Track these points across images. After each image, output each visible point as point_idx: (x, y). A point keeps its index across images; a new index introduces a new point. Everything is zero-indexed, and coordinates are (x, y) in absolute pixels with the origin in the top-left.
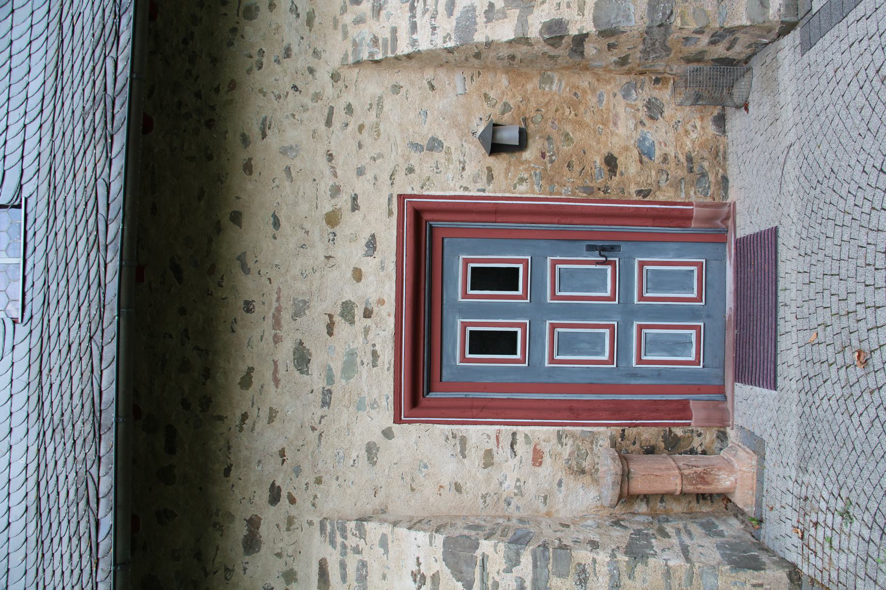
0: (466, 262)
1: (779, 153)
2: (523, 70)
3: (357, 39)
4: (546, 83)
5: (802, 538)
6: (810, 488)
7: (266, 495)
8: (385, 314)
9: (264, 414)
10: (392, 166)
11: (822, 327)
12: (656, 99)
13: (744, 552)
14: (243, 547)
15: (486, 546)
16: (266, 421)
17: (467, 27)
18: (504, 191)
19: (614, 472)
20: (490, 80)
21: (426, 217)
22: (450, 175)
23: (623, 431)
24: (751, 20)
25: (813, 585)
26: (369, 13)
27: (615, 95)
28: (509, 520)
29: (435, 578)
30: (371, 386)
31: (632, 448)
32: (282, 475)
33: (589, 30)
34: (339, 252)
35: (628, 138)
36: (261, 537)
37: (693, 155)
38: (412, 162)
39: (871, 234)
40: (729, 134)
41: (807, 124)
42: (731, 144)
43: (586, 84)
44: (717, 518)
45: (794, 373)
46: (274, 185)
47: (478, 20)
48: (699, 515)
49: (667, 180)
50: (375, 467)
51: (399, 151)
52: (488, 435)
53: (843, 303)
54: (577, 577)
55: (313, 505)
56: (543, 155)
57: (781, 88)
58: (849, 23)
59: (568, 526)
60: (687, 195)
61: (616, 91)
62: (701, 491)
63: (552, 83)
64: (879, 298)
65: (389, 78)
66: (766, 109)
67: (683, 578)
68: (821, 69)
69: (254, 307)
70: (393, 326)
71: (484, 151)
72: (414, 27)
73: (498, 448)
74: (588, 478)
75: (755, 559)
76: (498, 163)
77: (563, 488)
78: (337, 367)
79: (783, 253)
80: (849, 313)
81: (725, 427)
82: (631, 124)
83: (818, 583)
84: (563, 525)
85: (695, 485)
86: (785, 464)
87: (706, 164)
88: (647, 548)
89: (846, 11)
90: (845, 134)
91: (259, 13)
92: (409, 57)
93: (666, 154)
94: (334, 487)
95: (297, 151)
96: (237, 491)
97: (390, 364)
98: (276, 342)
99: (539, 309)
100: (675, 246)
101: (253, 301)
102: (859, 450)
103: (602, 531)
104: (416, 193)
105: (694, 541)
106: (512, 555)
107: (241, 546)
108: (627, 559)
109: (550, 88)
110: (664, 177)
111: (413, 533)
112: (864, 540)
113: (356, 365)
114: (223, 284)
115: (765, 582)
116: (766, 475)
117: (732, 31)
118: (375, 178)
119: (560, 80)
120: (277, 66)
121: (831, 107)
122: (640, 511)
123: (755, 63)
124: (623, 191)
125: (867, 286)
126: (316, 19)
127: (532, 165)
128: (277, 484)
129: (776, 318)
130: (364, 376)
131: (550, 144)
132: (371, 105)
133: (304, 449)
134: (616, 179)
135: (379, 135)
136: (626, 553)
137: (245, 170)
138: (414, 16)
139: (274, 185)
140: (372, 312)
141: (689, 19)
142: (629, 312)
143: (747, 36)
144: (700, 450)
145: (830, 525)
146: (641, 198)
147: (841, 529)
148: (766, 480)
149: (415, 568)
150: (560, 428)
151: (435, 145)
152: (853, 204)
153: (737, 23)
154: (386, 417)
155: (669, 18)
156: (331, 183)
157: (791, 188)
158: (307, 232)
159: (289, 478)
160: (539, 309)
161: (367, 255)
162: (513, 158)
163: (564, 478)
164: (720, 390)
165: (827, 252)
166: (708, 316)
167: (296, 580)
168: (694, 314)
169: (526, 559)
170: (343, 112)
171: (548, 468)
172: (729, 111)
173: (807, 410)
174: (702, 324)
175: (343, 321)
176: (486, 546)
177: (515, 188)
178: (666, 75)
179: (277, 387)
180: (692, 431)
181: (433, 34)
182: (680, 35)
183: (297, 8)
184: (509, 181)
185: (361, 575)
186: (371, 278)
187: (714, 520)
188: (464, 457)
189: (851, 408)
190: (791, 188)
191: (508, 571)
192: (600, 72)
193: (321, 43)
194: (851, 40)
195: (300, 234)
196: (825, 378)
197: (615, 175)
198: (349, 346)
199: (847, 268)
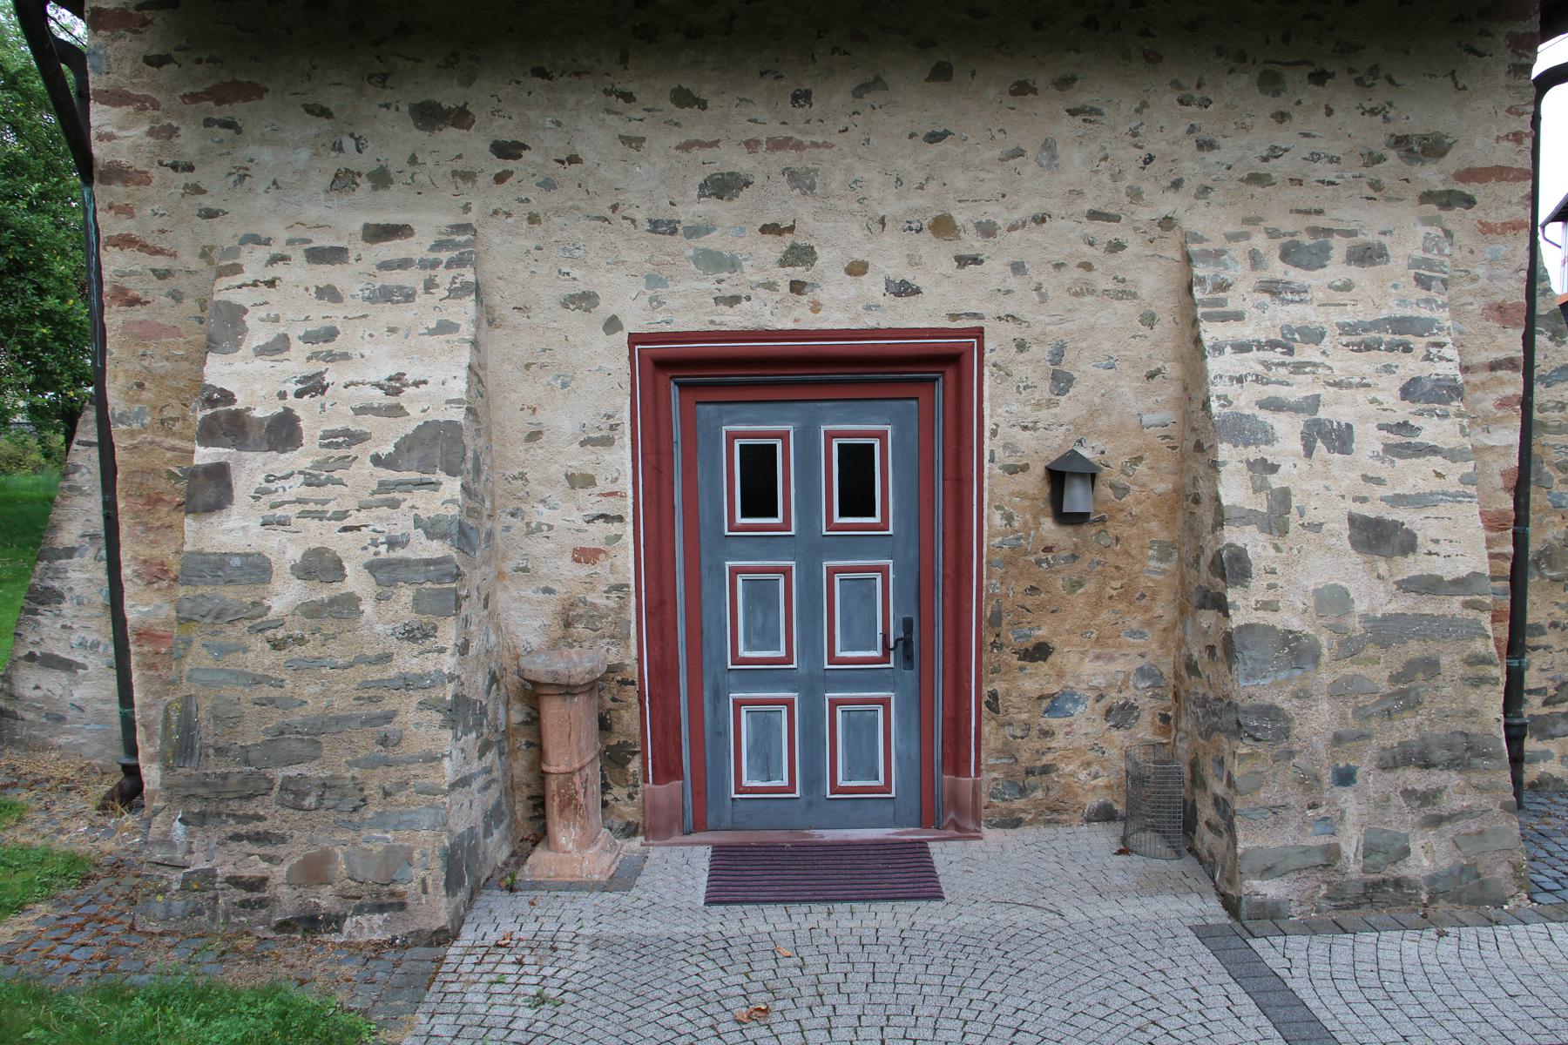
0: (882, 436)
1: (1051, 900)
2: (1179, 515)
3: (1225, 257)
4: (1160, 550)
5: (498, 946)
6: (570, 953)
7: (507, 136)
8: (796, 314)
9: (634, 129)
10: (1028, 317)
11: (800, 963)
12: (1137, 718)
13: (467, 867)
14: (422, 103)
15: (452, 487)
16: (623, 132)
17: (1241, 432)
18: (991, 492)
19: (573, 673)
20: (1163, 464)
21: (950, 372)
22: (1015, 407)
23: (633, 683)
24: (1244, 855)
25: (433, 961)
26: (1266, 275)
27: (1142, 656)
28: (490, 516)
29: (397, 411)
30: (686, 296)
31: (607, 697)
32: (539, 160)
33: (1234, 618)
35: (1078, 678)
36: (440, 130)
37: (1053, 775)
38: (1034, 348)
39: (930, 1021)
40: (1085, 828)
41: (1091, 936)
42: (1070, 830)
43: (1160, 612)
44: (509, 827)
45: (733, 928)
46: (995, 131)
47: (1253, 448)
48: (511, 800)
49: (1015, 737)
50: (559, 306)
51: (1051, 328)
52: (617, 479)
53: (834, 988)
54: (415, 626)
55: (495, 212)
56: (1048, 549)
57: (1146, 900)
58: (1226, 986)
59: (486, 607)
60: (992, 768)
61: (1149, 657)
62: (549, 801)
63: (1160, 560)
64: (843, 1033)
65: (1166, 309)
66: (1117, 880)
67: (426, 781)
68: (1168, 952)
69: (802, 106)
70: (779, 327)
71: (1053, 459)
72: (1242, 348)
73: (599, 495)
74: (558, 632)
75: (460, 883)
76: (1034, 482)
77: (541, 595)
78: (713, 242)
79: (905, 909)
80: (821, 996)
81: (644, 833)
82: (1099, 681)
83: (438, 968)
84: (486, 600)
85: (559, 793)
86: (599, 919)
87: (1039, 794)
88: (465, 726)
89: (1244, 982)
90: (1072, 985)
91: (1269, 97)
92: (1197, 341)
93: (1053, 734)
94: (525, 243)
95: (1049, 167)
96: (510, 89)
97: (721, 324)
98: (747, 143)
99: (812, 549)
100: (915, 751)
101: (811, 105)
102: (631, 1014)
103: (482, 658)
104: (987, 355)
105: (477, 795)
106: (443, 527)
107: (424, 99)
108: (449, 698)
109: (1152, 558)
110: (1019, 733)
111: (463, 373)
112: (510, 1022)
113: (717, 271)
114: (837, 55)
115: (431, 897)
116: (580, 894)
117: (1231, 828)
118: (1008, 292)
119: (1164, 572)
120: (1184, 128)
121: (1111, 967)
122: (512, 712)
123: (1189, 863)
124: (995, 671)
125: (859, 1017)
126: (1260, 189)
127: (1032, 533)
128: (525, 153)
129: (810, 901)
130: (701, 285)
131: (1065, 560)
132: (1123, 281)
133: (583, 195)
134: (1014, 661)
135: (1076, 294)
136: (456, 696)
137: (1018, 83)
138: (1260, 347)
139: (995, 131)
140: (800, 293)
141: (1249, 765)
142: (812, 685)
143: (1224, 850)
144: (608, 797)
145: (522, 981)
146: (986, 698)
147: (518, 995)
148: (573, 894)
149: (409, 378)
150: (633, 588)
152: (974, 997)
153: (1240, 835)
154: (638, 320)
155: (1250, 736)
156: (999, 222)
157: (998, 917)
158: (921, 187)
159: (535, 171)
160: (812, 549)
161: (888, 282)
162: (1043, 504)
163: (557, 595)
164: (700, 825)
165: (906, 967)
166: (810, 804)
167: (375, 188)
168: (812, 781)
169: (437, 549)
171: (569, 572)
172: (1119, 827)
173: (681, 946)
174: (797, 794)
175: (784, 249)
176: (452, 487)
177: (997, 508)
178: (1174, 732)
179: (678, 148)
180: (636, 786)
181: (1231, 379)
182: (1227, 752)
183: (1277, 157)
184: (1007, 498)
185: (392, 293)
186: (853, 291)
187: (506, 822)
188: (583, 444)
189: (689, 1003)
190: (998, 917)
191: (418, 522)
192: (1178, 633)
193: (1221, 199)
194: (1202, 990)
195: (919, 177)
196: (728, 969)
197: (1019, 659)
198: (745, 260)
199: (883, 992)
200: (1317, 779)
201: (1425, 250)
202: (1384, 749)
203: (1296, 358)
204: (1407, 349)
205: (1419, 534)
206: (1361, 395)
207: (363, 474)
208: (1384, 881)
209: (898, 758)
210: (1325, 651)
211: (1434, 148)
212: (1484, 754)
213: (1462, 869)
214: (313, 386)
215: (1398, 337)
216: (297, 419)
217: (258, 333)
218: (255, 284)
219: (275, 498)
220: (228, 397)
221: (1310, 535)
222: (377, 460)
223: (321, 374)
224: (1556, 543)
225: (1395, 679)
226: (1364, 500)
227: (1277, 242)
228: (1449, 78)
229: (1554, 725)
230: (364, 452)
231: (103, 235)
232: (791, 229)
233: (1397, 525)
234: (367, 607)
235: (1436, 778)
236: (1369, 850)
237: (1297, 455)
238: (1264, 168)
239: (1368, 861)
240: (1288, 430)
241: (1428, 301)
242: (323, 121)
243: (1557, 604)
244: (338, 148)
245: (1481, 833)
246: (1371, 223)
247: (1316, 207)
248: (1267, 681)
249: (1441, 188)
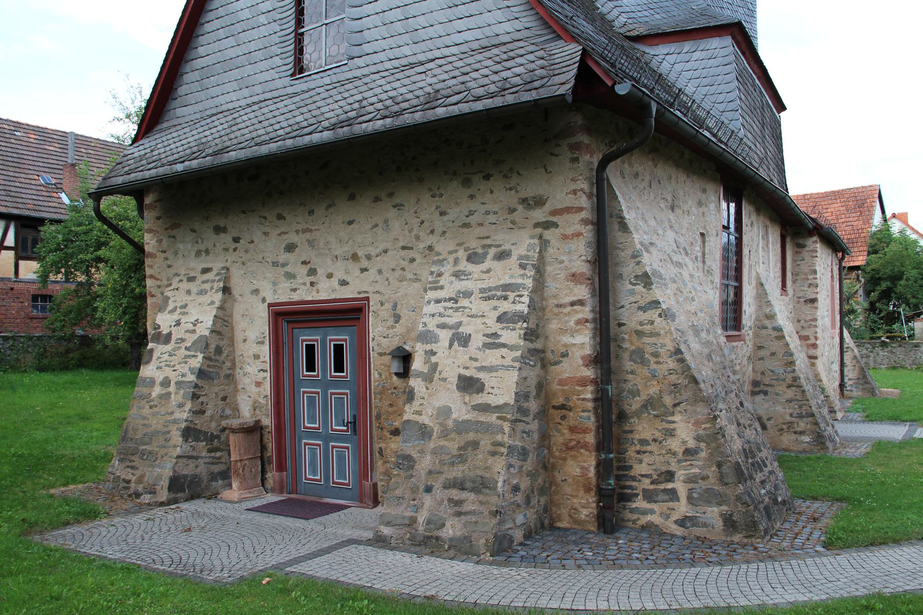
7: (236, 236)
10: (384, 292)
29: (194, 331)
34: (340, 263)
56: (395, 388)
72: (438, 301)
78: (288, 269)
118: (377, 282)
132: (416, 274)
134: (388, 435)
135: (400, 281)
151: (397, 318)
156: (372, 254)
161: (339, 280)
168: (327, 479)
170: (411, 256)
171: (253, 389)
177: (377, 370)
181: (430, 315)
193: (450, 236)
200: (418, 488)
201: (528, 251)
202: (447, 479)
203: (459, 305)
204: (506, 298)
205: (486, 384)
206: (479, 321)
208: (432, 536)
209: (353, 472)
210: (435, 434)
211: (539, 202)
212: (488, 487)
213: (465, 538)
215: (504, 293)
221: (442, 383)
222: (186, 349)
224: (655, 396)
225: (460, 449)
226: (467, 368)
228: (543, 169)
229: (657, 495)
230: (183, 345)
232: (309, 262)
233: (478, 380)
234: (173, 396)
235: (464, 495)
236: (429, 522)
238: (468, 220)
239: (428, 527)
240: (445, 336)
241: (523, 275)
243: (657, 429)
244: (197, 243)
245: (476, 522)
246: (504, 239)
247: (487, 235)
248: (410, 445)
249: (544, 220)
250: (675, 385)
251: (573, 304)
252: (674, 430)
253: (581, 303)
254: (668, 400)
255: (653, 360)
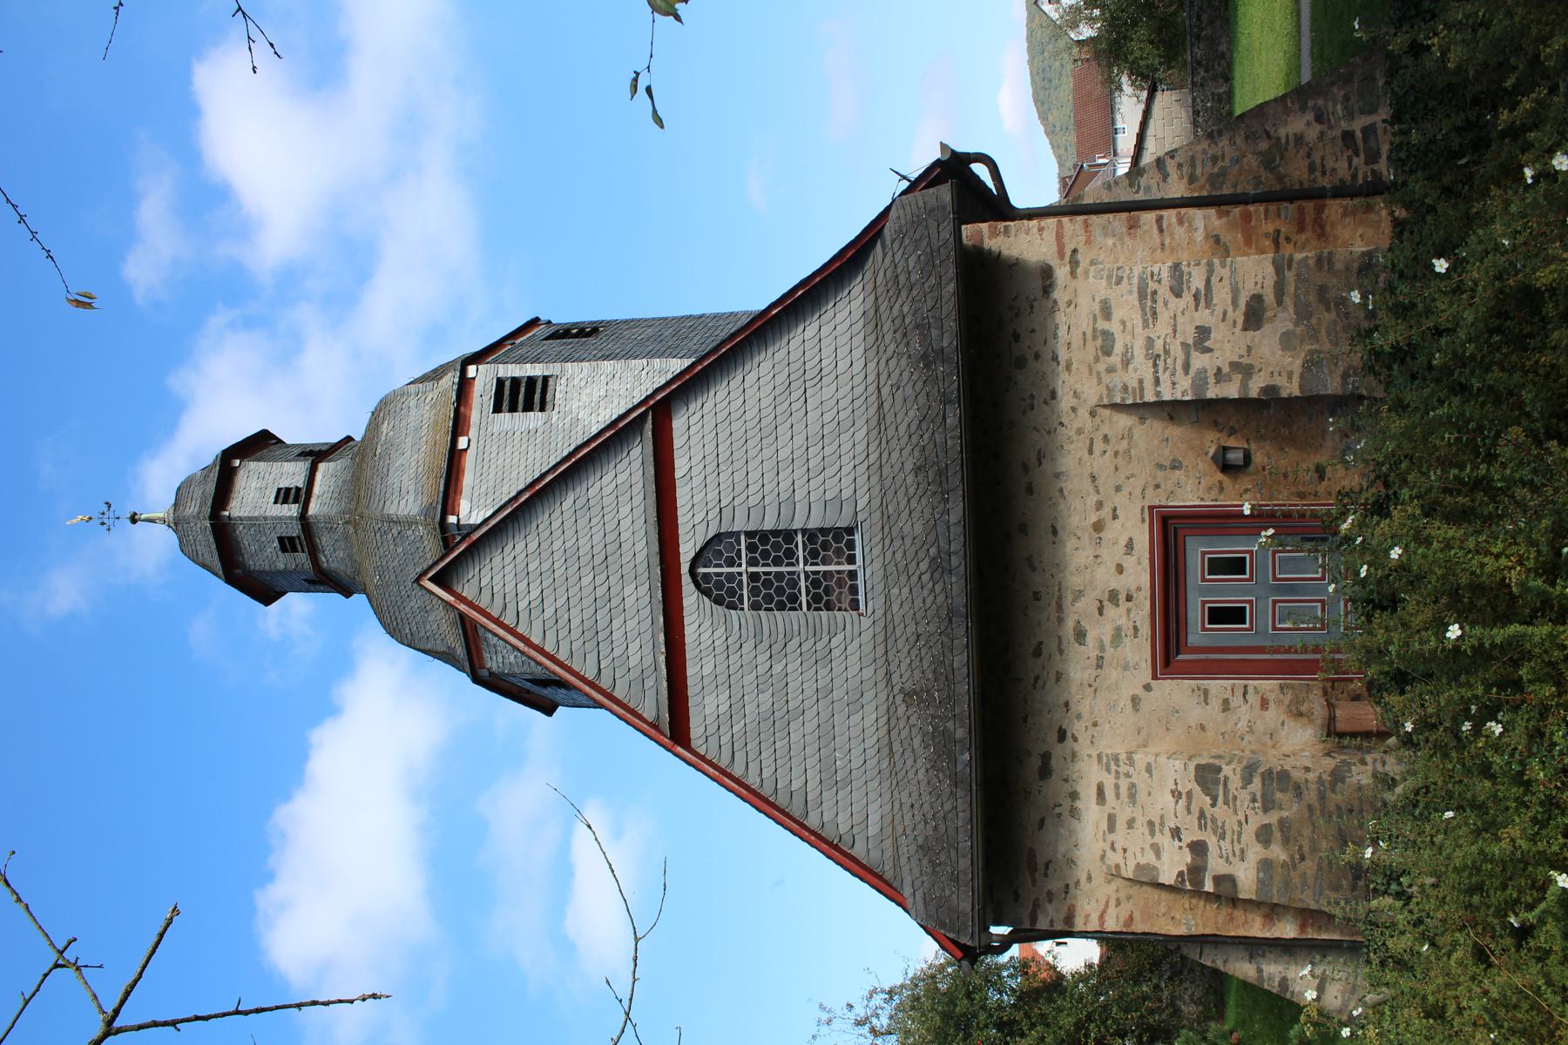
0: (1204, 554)
8: (1143, 599)
9: (1052, 676)
29: (1189, 794)
34: (1104, 552)
59: (1289, 756)
72: (1157, 381)
74: (1305, 720)
77: (1285, 727)
84: (1285, 755)
98: (1059, 622)
104: (1162, 504)
111: (1171, 761)
120: (1045, 407)
130: (1128, 644)
135: (1130, 458)
138: (1157, 372)
149: (1174, 787)
154: (1145, 674)
181: (1173, 388)
188: (1207, 704)
191: (1244, 787)
201: (1102, 278)
203: (1162, 353)
204: (1155, 293)
206: (1180, 320)
207: (1220, 811)
210: (1314, 347)
214: (1176, 833)
216: (1192, 842)
217: (1149, 858)
218: (1125, 858)
219: (1231, 855)
220: (1181, 874)
221: (1253, 352)
222: (1213, 805)
223: (1170, 829)
225: (1328, 309)
226: (1235, 322)
227: (1102, 358)
230: (1209, 811)
231: (1098, 929)
232: (1101, 601)
233: (1248, 305)
234: (1285, 814)
237: (1211, 357)
240: (1199, 361)
241: (1129, 278)
242: (1046, 822)
244: (1059, 815)
250: (1247, 138)
251: (1161, 230)
252: (1295, 135)
253: (1159, 220)
254: (1264, 145)
255: (1220, 164)
